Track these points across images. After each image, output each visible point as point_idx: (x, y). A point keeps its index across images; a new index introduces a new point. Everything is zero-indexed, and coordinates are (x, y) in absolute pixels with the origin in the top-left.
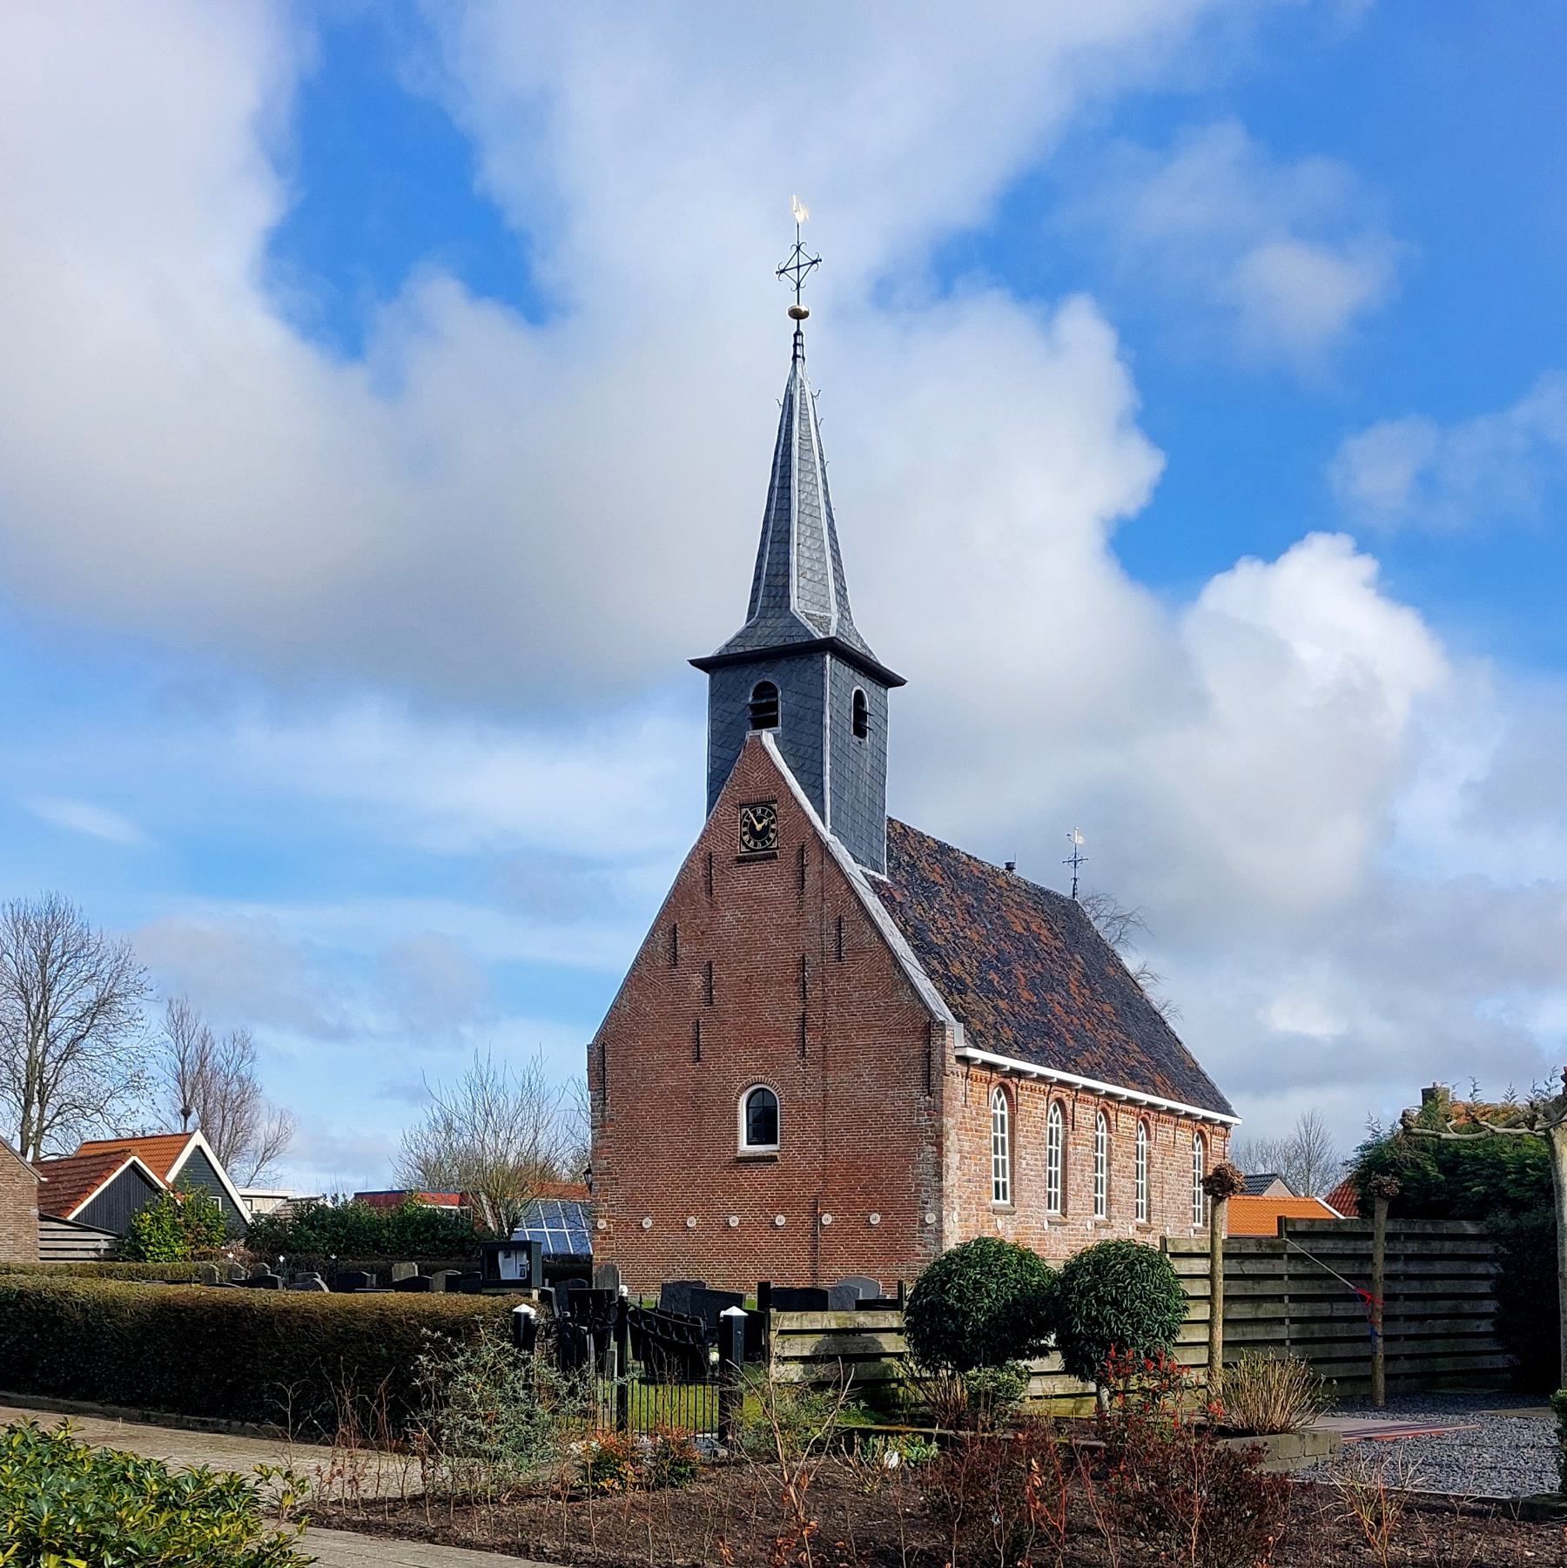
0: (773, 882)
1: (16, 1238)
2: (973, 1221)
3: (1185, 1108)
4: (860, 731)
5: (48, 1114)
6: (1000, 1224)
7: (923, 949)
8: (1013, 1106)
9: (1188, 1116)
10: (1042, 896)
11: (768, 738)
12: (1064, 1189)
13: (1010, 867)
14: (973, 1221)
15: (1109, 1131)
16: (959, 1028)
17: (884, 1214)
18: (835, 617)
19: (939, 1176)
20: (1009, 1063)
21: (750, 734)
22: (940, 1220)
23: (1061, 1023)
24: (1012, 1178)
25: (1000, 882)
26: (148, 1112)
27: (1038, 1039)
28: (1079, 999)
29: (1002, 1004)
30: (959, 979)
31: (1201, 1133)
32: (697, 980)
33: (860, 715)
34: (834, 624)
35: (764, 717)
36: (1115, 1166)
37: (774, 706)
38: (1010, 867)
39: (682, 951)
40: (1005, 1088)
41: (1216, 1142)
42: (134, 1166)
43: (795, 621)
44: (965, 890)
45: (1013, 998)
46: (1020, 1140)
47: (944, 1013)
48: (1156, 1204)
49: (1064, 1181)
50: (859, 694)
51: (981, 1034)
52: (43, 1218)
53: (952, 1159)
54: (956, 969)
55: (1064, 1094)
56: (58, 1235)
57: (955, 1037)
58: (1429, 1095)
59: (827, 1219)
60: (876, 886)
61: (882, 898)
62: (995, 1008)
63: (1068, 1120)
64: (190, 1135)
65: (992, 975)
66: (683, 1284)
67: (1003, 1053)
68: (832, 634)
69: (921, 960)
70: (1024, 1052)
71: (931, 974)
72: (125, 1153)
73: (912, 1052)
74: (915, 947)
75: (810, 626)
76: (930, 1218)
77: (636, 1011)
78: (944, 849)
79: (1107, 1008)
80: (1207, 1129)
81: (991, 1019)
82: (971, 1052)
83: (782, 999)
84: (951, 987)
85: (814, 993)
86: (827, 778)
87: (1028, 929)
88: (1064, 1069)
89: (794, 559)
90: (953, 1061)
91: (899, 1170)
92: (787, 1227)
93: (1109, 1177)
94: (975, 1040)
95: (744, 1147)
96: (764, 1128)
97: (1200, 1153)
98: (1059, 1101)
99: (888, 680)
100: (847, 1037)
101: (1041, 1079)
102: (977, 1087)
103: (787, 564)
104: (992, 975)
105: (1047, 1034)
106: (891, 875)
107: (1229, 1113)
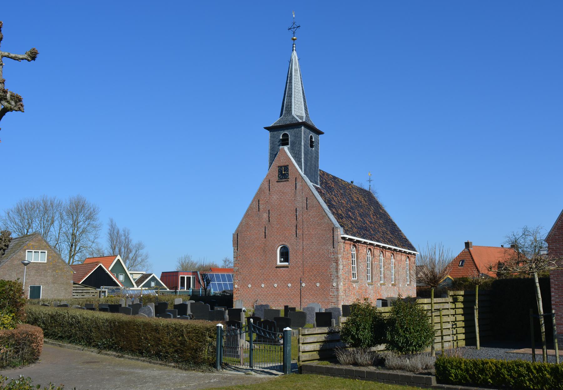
0: (287, 187)
1: (66, 290)
2: (347, 285)
3: (404, 250)
4: (312, 146)
5: (77, 249)
6: (354, 285)
7: (330, 206)
8: (357, 251)
9: (405, 252)
10: (361, 191)
11: (286, 148)
12: (372, 274)
13: (352, 182)
14: (347, 285)
15: (384, 257)
16: (342, 229)
17: (321, 283)
18: (304, 115)
19: (337, 272)
20: (356, 238)
21: (281, 147)
22: (337, 285)
23: (369, 226)
24: (357, 272)
25: (350, 187)
26: (103, 244)
27: (363, 231)
28: (373, 219)
29: (353, 221)
30: (341, 215)
31: (408, 257)
32: (265, 215)
33: (312, 142)
34: (304, 118)
35: (285, 142)
36: (385, 267)
37: (288, 140)
38: (352, 182)
39: (261, 207)
40: (354, 245)
41: (412, 259)
42: (100, 266)
43: (293, 117)
44: (341, 189)
45: (356, 219)
46: (360, 261)
47: (337, 225)
48: (397, 277)
49: (372, 272)
50: (311, 137)
51: (348, 230)
52: (74, 284)
53: (341, 267)
54: (340, 212)
55: (371, 247)
56: (78, 289)
57: (341, 233)
58: (467, 245)
59: (304, 285)
60: (317, 189)
61: (318, 192)
62: (351, 222)
63: (373, 255)
64: (117, 256)
65: (350, 213)
66: (262, 305)
67: (354, 236)
68: (304, 120)
69: (330, 209)
70: (360, 235)
71: (333, 213)
72: (97, 263)
73: (328, 236)
74: (328, 206)
75: (298, 118)
76: (335, 284)
77: (247, 224)
78: (334, 178)
79: (381, 222)
80: (410, 256)
81: (350, 226)
82: (345, 236)
83: (290, 220)
84: (339, 217)
85: (299, 218)
86: (303, 159)
87: (358, 200)
88: (371, 240)
89: (293, 101)
90: (340, 238)
91: (325, 271)
92: (291, 287)
93: (384, 271)
94: (346, 232)
95: (279, 263)
96: (285, 255)
97: (408, 262)
98: (370, 249)
99: (319, 133)
100: (309, 231)
101: (365, 243)
102: (348, 246)
103: (291, 102)
104: (350, 213)
105: (366, 230)
106: (320, 185)
107: (414, 250)
